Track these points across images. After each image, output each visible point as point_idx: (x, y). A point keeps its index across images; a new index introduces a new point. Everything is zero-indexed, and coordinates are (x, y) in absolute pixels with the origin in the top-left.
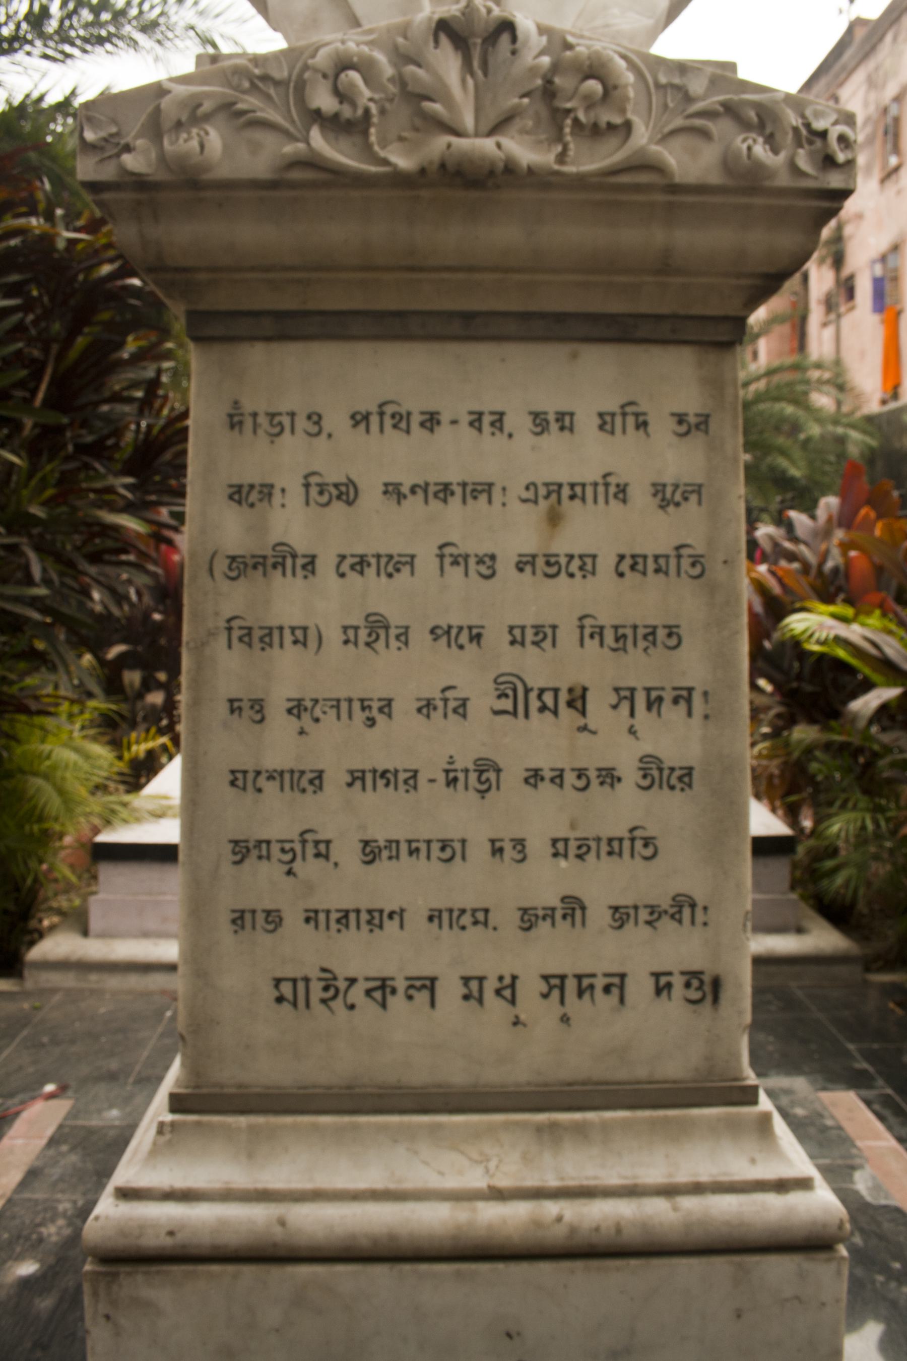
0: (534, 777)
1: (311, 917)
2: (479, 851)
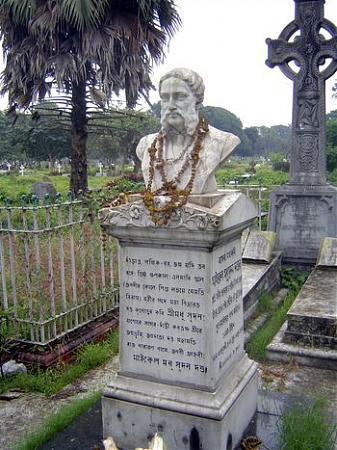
0: (174, 327)
1: (139, 345)
2: (166, 338)
